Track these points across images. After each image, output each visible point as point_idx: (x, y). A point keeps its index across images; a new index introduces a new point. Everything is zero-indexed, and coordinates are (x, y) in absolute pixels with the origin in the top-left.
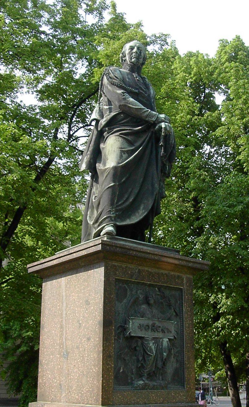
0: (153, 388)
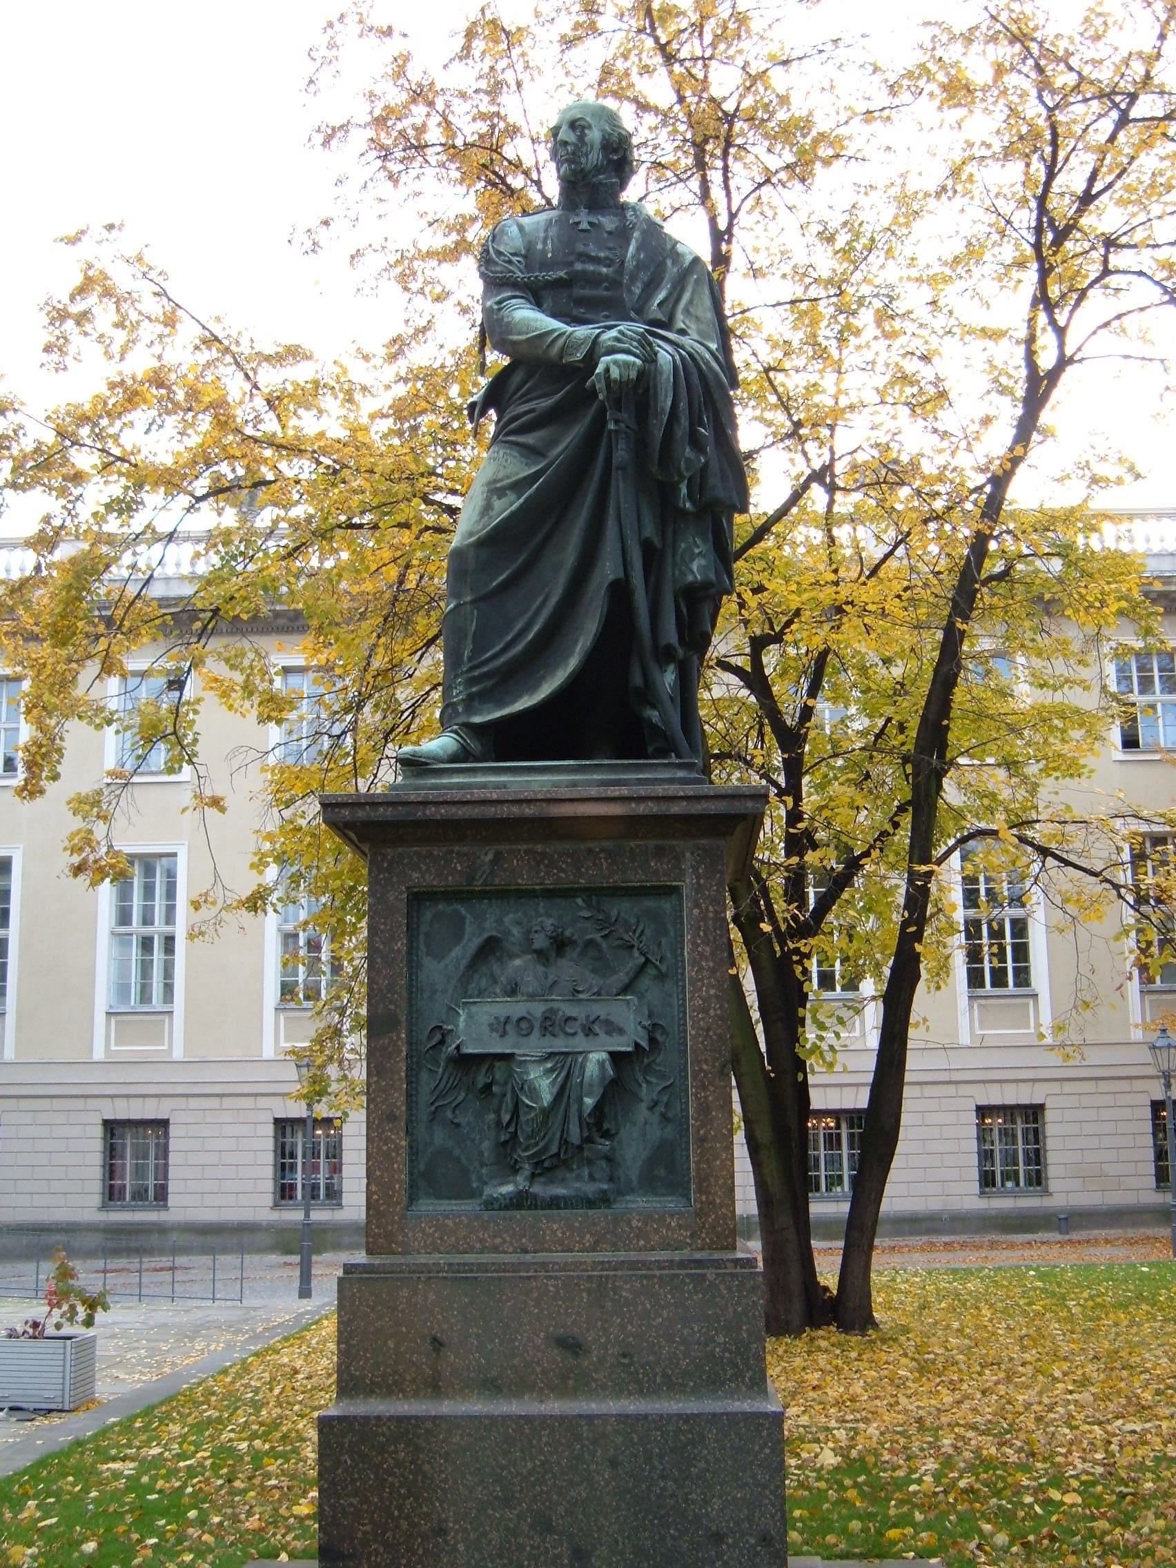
0: (554, 1203)
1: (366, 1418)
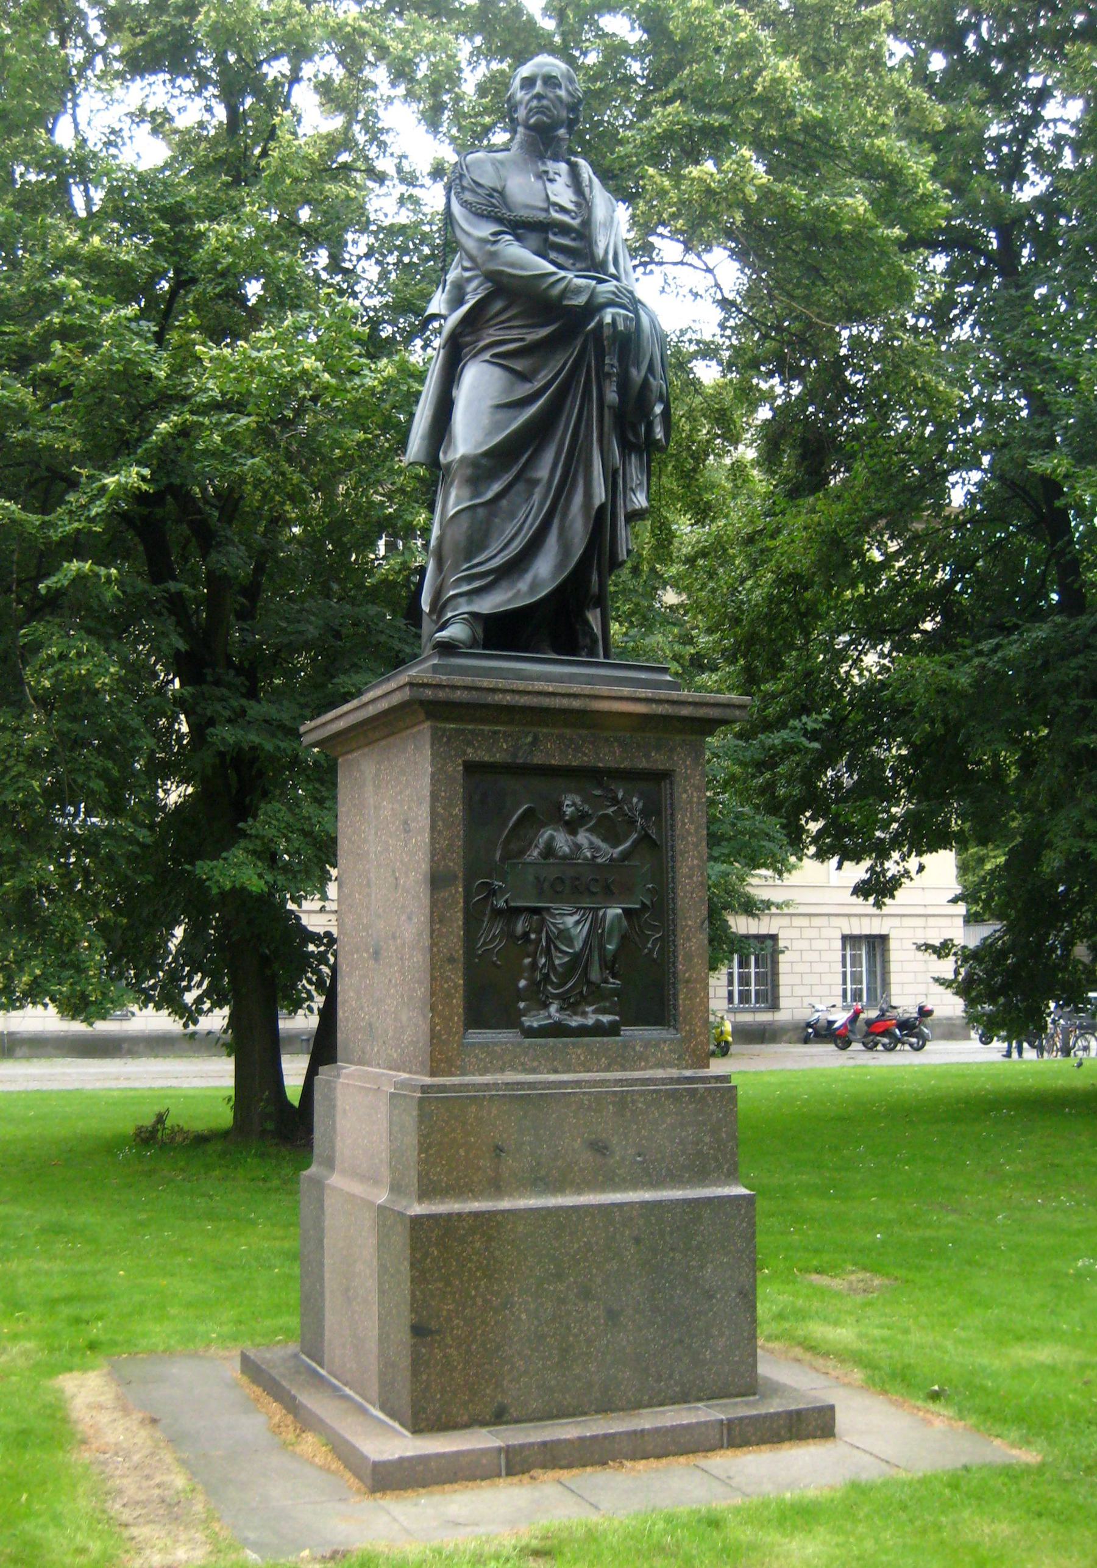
1: (450, 1215)
